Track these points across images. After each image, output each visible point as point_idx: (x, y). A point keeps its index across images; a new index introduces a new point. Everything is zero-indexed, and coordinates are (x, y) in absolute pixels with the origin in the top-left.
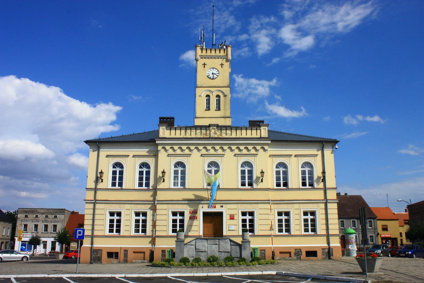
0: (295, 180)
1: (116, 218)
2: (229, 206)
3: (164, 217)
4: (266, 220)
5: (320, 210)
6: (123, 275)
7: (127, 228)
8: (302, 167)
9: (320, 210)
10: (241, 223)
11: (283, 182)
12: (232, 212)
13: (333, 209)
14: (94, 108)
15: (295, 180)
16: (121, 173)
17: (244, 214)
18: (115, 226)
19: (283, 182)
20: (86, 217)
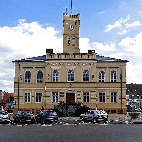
0: (108, 78)
1: (102, 95)
2: (78, 90)
3: (49, 95)
4: (94, 96)
5: (118, 92)
6: (17, 126)
7: (108, 100)
8: (84, 73)
9: (118, 92)
10: (111, 98)
11: (102, 80)
12: (79, 93)
13: (124, 91)
14: (115, 54)
15: (108, 78)
16: (57, 75)
17: (84, 94)
18: (28, 99)
19: (102, 80)
20: (15, 95)
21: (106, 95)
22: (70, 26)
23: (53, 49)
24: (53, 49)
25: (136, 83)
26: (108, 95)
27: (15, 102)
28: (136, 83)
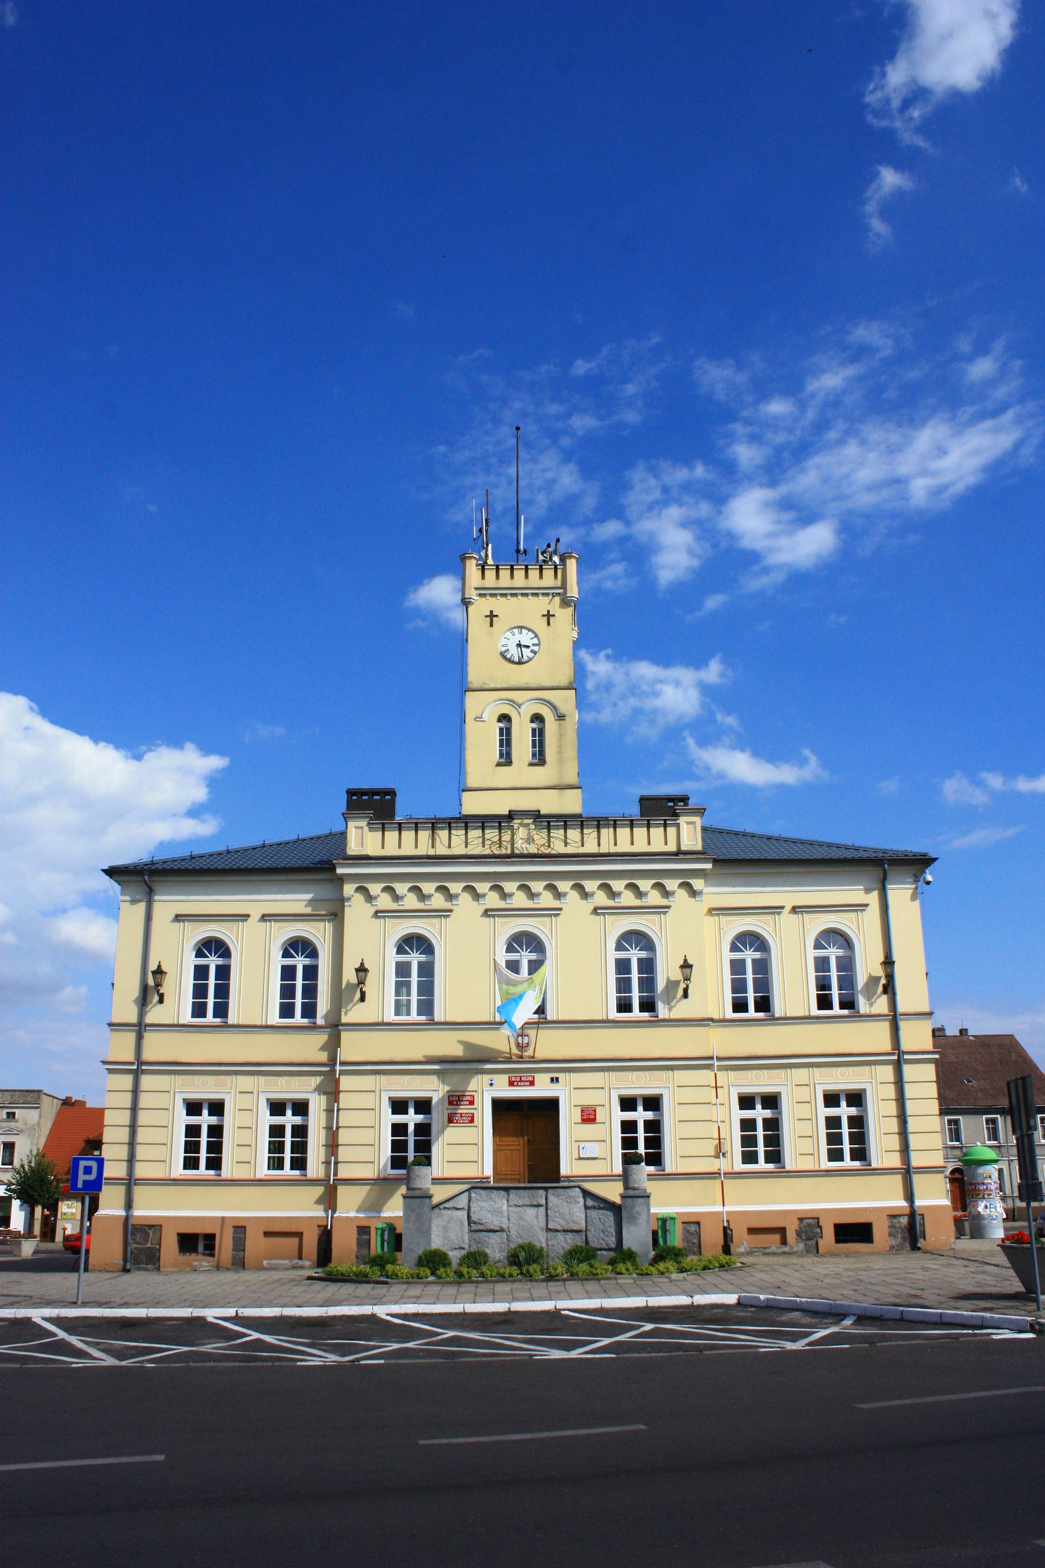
0: (793, 989)
3: (367, 1118)
5: (876, 1086)
7: (245, 1154)
8: (507, 951)
9: (876, 1086)
10: (823, 1131)
12: (589, 1099)
15: (793, 989)
16: (224, 972)
18: (205, 1148)
20: (109, 1118)
21: (230, 1121)
22: (508, 634)
23: (392, 793)
24: (392, 793)
25: (963, 1032)
26: (246, 1119)
27: (94, 1165)
28: (963, 1032)
